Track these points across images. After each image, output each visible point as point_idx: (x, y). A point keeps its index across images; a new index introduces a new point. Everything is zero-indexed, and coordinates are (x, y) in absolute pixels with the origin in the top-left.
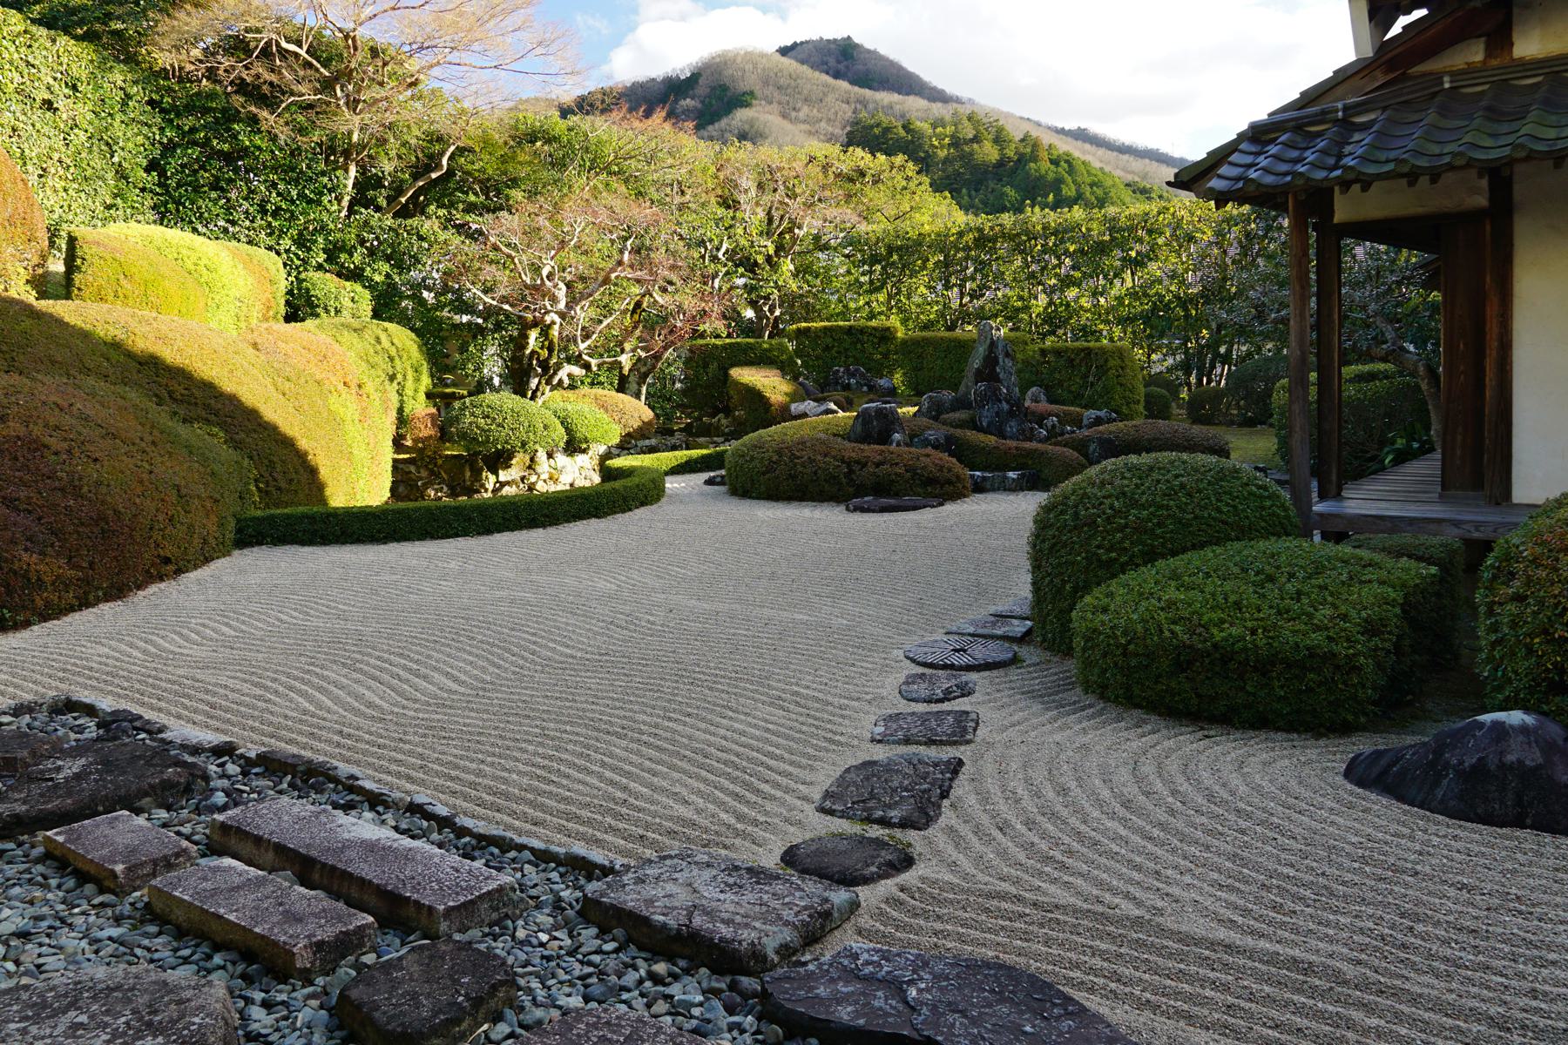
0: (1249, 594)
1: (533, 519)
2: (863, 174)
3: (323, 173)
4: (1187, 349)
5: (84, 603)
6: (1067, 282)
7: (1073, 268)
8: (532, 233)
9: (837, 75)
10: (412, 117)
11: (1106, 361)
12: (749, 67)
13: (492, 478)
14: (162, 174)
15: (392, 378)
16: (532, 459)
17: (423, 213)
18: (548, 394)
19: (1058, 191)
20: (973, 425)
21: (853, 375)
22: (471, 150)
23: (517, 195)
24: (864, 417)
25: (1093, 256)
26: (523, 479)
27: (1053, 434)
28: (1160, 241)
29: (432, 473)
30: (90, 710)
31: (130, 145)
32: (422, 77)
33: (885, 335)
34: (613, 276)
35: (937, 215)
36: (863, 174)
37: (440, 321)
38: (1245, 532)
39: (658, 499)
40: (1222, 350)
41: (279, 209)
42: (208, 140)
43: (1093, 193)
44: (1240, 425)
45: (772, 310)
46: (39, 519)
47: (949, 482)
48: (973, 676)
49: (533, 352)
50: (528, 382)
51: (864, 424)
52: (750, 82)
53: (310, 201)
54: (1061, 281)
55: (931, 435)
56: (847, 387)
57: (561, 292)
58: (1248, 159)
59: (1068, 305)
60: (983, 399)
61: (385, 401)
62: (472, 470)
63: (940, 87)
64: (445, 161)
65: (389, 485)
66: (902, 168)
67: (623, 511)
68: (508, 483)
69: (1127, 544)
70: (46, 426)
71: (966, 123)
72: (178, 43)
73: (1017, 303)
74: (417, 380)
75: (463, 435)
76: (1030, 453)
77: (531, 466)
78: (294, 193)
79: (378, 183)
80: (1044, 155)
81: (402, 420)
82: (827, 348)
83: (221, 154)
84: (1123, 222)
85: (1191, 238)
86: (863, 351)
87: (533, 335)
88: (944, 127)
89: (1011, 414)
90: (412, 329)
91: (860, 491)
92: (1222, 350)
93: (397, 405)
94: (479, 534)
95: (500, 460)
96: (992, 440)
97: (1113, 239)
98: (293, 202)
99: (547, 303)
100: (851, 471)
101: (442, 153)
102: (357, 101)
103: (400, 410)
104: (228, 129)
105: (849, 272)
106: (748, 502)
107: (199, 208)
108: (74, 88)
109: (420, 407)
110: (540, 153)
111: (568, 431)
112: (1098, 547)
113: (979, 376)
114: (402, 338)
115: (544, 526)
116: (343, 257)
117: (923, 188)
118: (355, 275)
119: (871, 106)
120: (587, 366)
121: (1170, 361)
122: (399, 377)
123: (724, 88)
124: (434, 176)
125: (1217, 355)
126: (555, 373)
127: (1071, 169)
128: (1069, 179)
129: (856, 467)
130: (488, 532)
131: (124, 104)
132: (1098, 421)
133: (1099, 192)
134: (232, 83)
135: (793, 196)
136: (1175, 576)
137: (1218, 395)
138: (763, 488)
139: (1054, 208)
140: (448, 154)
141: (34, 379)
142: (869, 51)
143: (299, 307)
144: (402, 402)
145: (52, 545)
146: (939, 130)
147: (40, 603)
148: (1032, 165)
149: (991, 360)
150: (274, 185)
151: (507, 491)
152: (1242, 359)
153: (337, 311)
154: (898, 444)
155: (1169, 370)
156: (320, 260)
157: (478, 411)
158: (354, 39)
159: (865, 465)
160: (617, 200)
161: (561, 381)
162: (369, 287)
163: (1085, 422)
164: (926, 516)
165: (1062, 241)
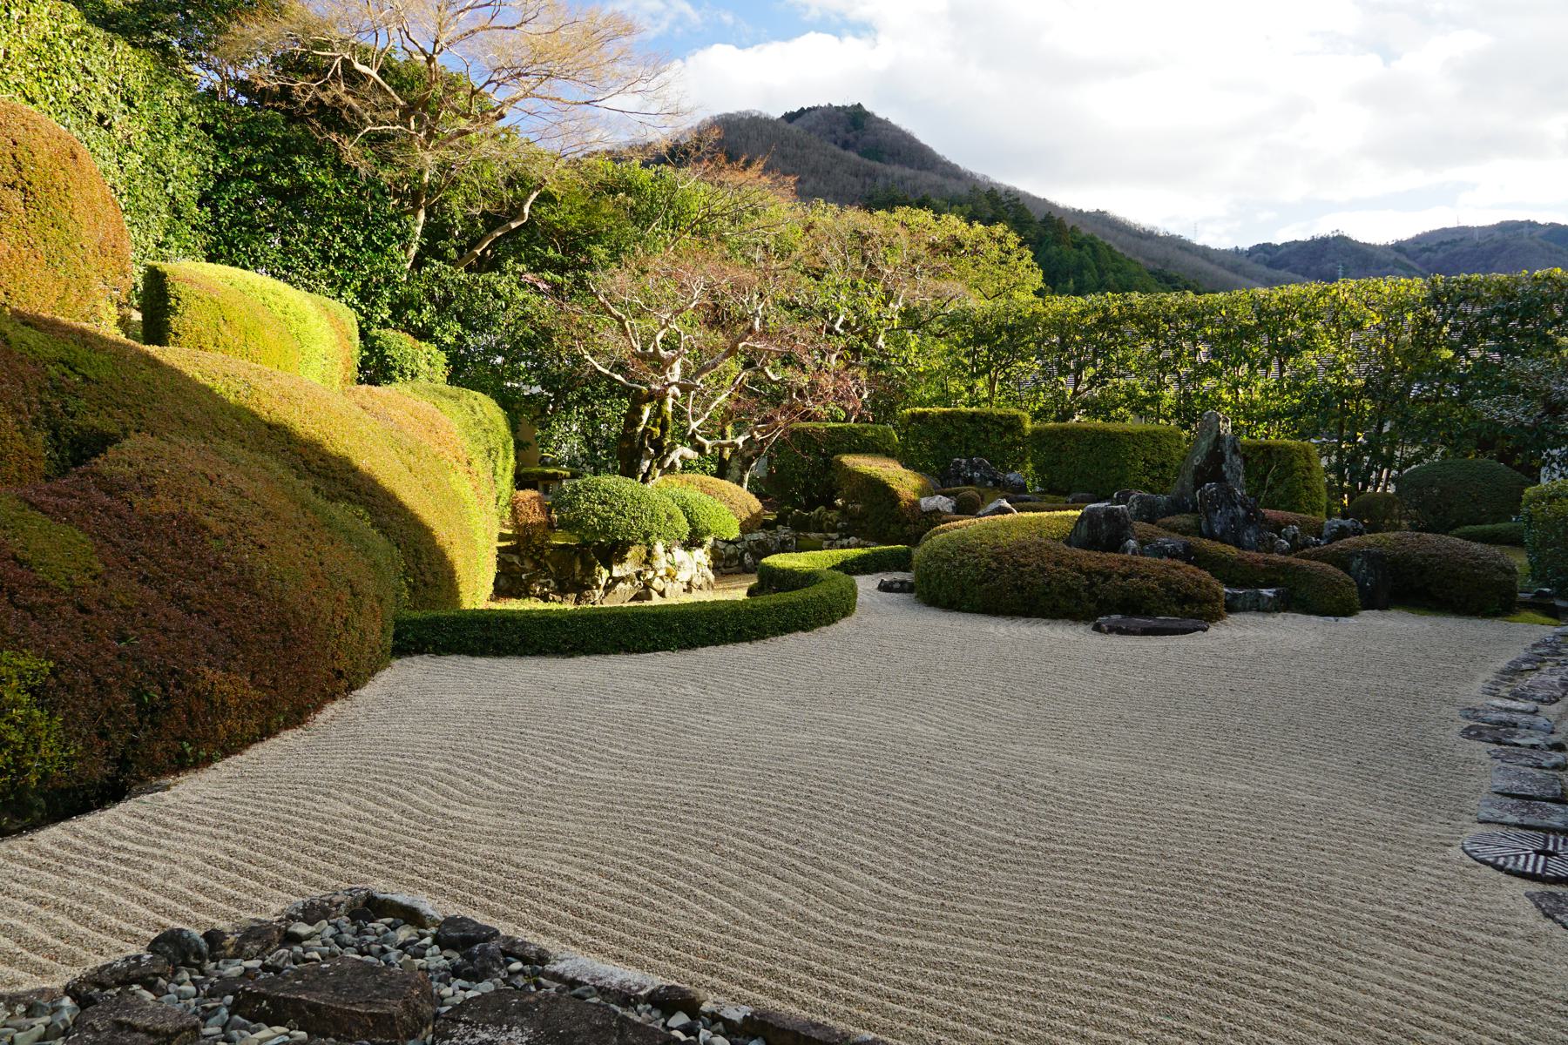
2: (961, 246)
3: (392, 218)
5: (267, 733)
9: (846, 145)
10: (486, 155)
11: (1292, 460)
13: (605, 573)
14: (215, 211)
16: (649, 553)
17: (499, 268)
18: (658, 478)
21: (977, 468)
23: (600, 252)
25: (1232, 343)
26: (639, 574)
27: (1296, 547)
28: (1318, 326)
29: (537, 564)
30: (411, 916)
31: (185, 174)
34: (741, 345)
41: (343, 256)
42: (265, 173)
46: (217, 623)
49: (645, 430)
50: (638, 465)
53: (377, 249)
59: (1205, 397)
62: (582, 563)
63: (953, 162)
64: (526, 210)
68: (622, 579)
70: (200, 501)
72: (252, 50)
76: (1282, 568)
78: (360, 239)
82: (947, 436)
83: (279, 193)
86: (986, 441)
87: (647, 411)
89: (1248, 520)
91: (1105, 607)
94: (681, 648)
95: (613, 552)
96: (1232, 551)
97: (1260, 324)
98: (358, 249)
104: (289, 162)
107: (255, 251)
108: (131, 104)
115: (750, 640)
116: (411, 313)
118: (424, 334)
120: (700, 449)
124: (514, 225)
129: (1098, 579)
131: (179, 126)
134: (309, 104)
138: (978, 600)
139: (1077, 294)
141: (170, 442)
142: (879, 121)
143: (376, 368)
145: (234, 658)
147: (223, 733)
150: (339, 229)
153: (414, 376)
154: (1134, 553)
156: (385, 316)
157: (594, 496)
159: (1107, 577)
161: (673, 464)
163: (1326, 532)
165: (1201, 325)
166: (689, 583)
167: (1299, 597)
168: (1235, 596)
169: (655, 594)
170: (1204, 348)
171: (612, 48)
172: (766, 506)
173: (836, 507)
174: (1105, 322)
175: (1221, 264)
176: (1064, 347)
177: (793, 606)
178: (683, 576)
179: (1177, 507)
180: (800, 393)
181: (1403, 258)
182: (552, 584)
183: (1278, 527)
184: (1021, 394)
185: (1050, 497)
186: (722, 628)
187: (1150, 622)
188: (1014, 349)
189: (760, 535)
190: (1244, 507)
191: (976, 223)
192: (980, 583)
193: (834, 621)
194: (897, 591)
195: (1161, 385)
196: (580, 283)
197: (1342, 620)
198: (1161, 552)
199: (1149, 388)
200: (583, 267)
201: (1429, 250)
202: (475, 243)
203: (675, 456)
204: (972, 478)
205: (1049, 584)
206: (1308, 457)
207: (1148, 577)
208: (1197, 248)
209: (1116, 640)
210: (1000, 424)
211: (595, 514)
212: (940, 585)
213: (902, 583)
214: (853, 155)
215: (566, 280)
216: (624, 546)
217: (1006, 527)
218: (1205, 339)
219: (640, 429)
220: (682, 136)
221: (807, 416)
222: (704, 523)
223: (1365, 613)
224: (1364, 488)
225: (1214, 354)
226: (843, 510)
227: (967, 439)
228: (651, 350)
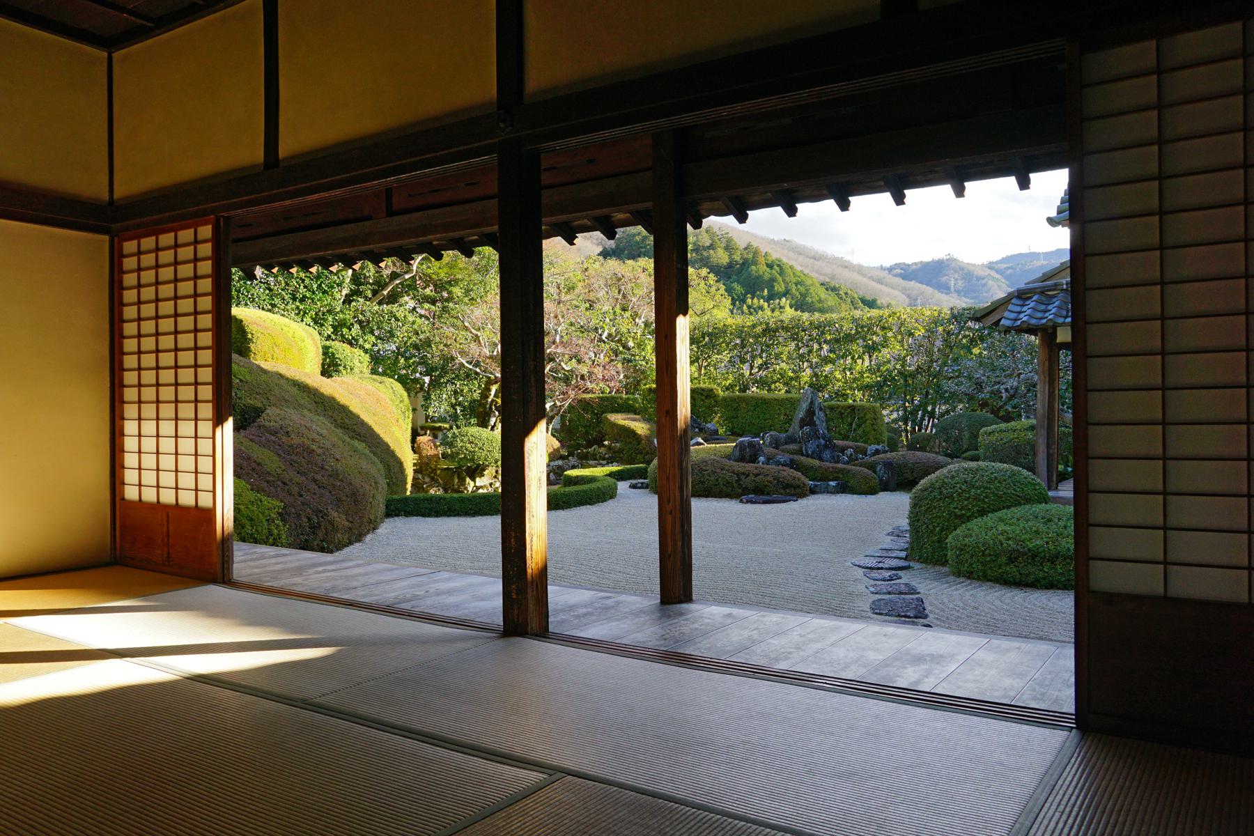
0: (1042, 528)
5: (350, 543)
6: (826, 360)
7: (831, 351)
13: (472, 484)
19: (771, 287)
20: (800, 452)
24: (741, 447)
25: (842, 341)
27: (851, 460)
28: (890, 334)
29: (433, 479)
38: (1028, 501)
40: (929, 408)
41: (304, 297)
47: (799, 487)
48: (900, 573)
53: (325, 292)
58: (1018, 309)
60: (809, 437)
66: (705, 279)
73: (789, 373)
76: (842, 470)
78: (315, 286)
80: (762, 260)
84: (865, 321)
85: (911, 334)
89: (826, 446)
91: (746, 491)
92: (929, 408)
96: (816, 462)
97: (858, 332)
100: (739, 480)
113: (803, 423)
115: (563, 508)
118: (352, 343)
121: (895, 415)
127: (782, 272)
128: (780, 279)
129: (743, 477)
132: (877, 452)
133: (802, 289)
136: (1001, 520)
149: (810, 412)
151: (481, 491)
152: (942, 415)
155: (895, 421)
165: (823, 333)
167: (844, 488)
170: (825, 347)
172: (563, 446)
173: (604, 446)
174: (767, 331)
175: (871, 278)
176: (743, 346)
177: (585, 492)
179: (791, 440)
180: (583, 377)
181: (993, 273)
183: (843, 450)
187: (768, 498)
188: (712, 346)
189: (560, 462)
195: (801, 370)
196: (444, 309)
198: (778, 463)
199: (794, 371)
200: (447, 300)
206: (875, 412)
208: (854, 266)
209: (749, 506)
215: (436, 308)
218: (825, 342)
221: (586, 391)
224: (920, 430)
226: (609, 448)
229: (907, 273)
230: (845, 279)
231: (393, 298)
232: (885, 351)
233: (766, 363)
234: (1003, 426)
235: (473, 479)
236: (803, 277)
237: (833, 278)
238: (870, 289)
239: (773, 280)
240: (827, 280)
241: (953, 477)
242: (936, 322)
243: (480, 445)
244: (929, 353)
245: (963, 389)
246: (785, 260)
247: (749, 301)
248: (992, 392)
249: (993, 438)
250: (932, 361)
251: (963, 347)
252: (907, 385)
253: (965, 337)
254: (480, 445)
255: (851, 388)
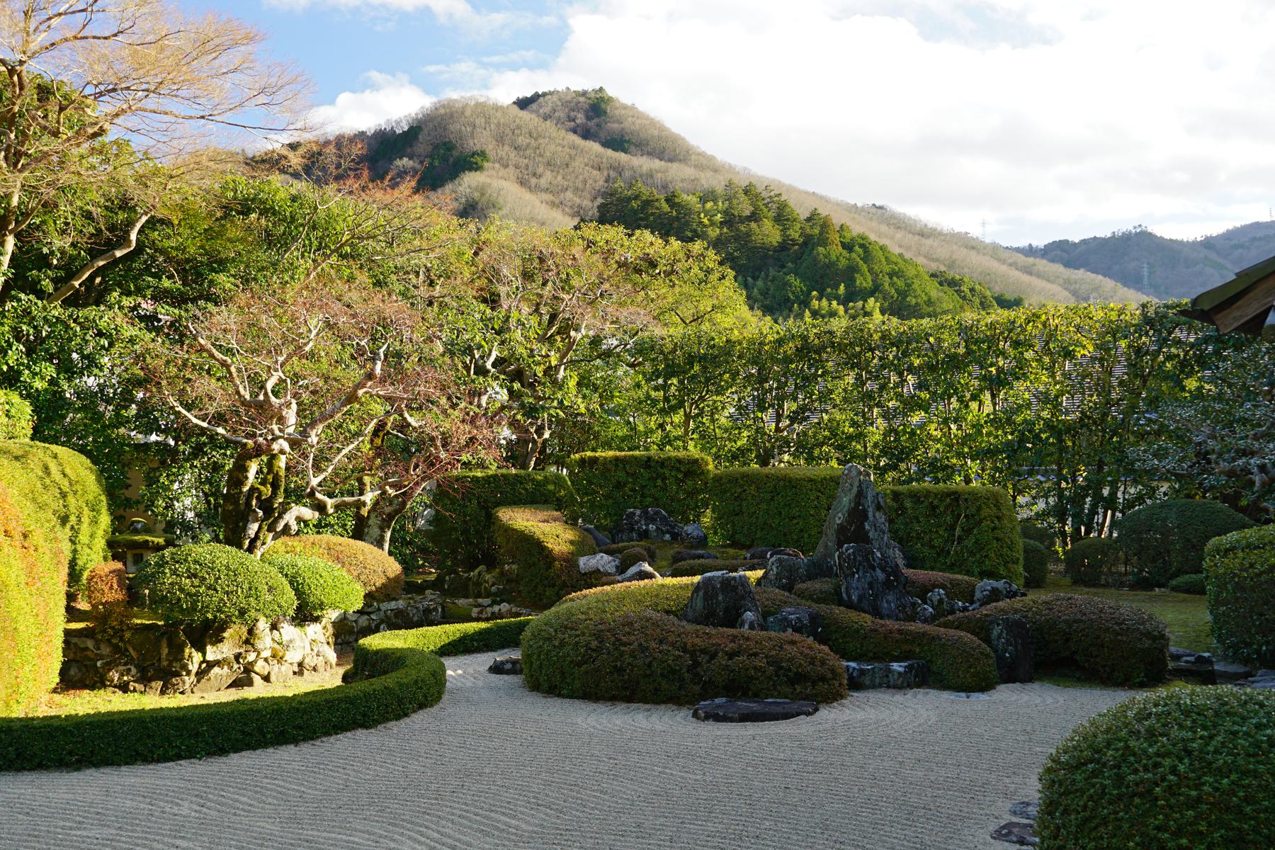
1: (282, 733)
2: (653, 265)
4: (1061, 491)
6: (912, 404)
8: (252, 329)
9: (586, 135)
11: (979, 509)
12: (480, 121)
13: (197, 657)
15: (64, 520)
16: (250, 632)
19: (850, 281)
22: (165, 222)
23: (224, 281)
25: (942, 371)
26: (237, 657)
28: (1029, 355)
29: (116, 649)
32: (107, 126)
33: (691, 468)
34: (361, 392)
35: (737, 319)
36: (653, 265)
37: (124, 442)
39: (438, 698)
40: (1106, 492)
43: (892, 284)
44: (1133, 587)
45: (540, 431)
47: (823, 679)
49: (252, 489)
50: (245, 529)
51: (705, 599)
52: (482, 140)
54: (905, 403)
55: (792, 613)
56: (645, 535)
57: (291, 416)
59: (913, 433)
61: (57, 553)
62: (170, 646)
63: (709, 152)
64: (133, 236)
65: (58, 666)
67: (398, 718)
68: (217, 663)
69: (1203, 827)
71: (742, 197)
73: (848, 433)
74: (94, 522)
75: (158, 600)
77: (249, 640)
79: (43, 262)
80: (835, 237)
81: (74, 575)
82: (619, 486)
85: (1069, 354)
86: (664, 489)
87: (253, 467)
88: (715, 201)
90: (82, 450)
91: (709, 690)
92: (1106, 492)
93: (69, 556)
94: (210, 754)
96: (867, 620)
97: (969, 352)
99: (275, 427)
100: (696, 664)
101: (130, 224)
102: (19, 155)
103: (73, 563)
105: (638, 386)
106: (558, 702)
109: (96, 559)
110: (248, 230)
111: (299, 593)
112: (1158, 828)
113: (843, 535)
114: (75, 466)
115: (295, 741)
117: (727, 282)
119: (627, 174)
120: (320, 507)
121: (1041, 505)
122: (73, 519)
123: (449, 146)
124: (118, 254)
125: (1098, 498)
126: (280, 516)
127: (867, 256)
128: (865, 268)
129: (703, 659)
130: (222, 751)
132: (995, 595)
133: (900, 283)
135: (566, 284)
137: (1106, 547)
138: (577, 684)
140: (138, 225)
142: (625, 107)
144: (75, 551)
146: (709, 205)
148: (821, 249)
149: (858, 514)
152: (1129, 504)
154: (752, 627)
155: (1041, 516)
157: (182, 569)
158: (19, 76)
159: (713, 656)
160: (362, 299)
161: (287, 527)
162: (28, 396)
163: (978, 595)
164: (801, 727)
165: (905, 354)
166: (300, 665)
167: (925, 676)
168: (862, 672)
169: (257, 679)
170: (911, 379)
171: (229, 59)
178: (293, 656)
179: (819, 570)
181: (1214, 256)
182: (134, 671)
183: (923, 591)
184: (713, 433)
185: (731, 551)
186: (260, 730)
187: (754, 706)
188: (710, 382)
190: (883, 570)
191: (672, 240)
192: (579, 665)
193: (406, 715)
194: (508, 672)
197: (975, 696)
199: (854, 424)
201: (1242, 246)
202: (72, 275)
203: (290, 518)
204: (646, 531)
205: (649, 665)
207: (756, 655)
208: (986, 246)
210: (678, 470)
211: (182, 590)
212: (540, 667)
213: (514, 662)
214: (595, 147)
216: (223, 626)
217: (620, 598)
218: (911, 369)
219: (245, 489)
220: (398, 123)
222: (316, 594)
223: (1002, 687)
224: (1088, 532)
225: (921, 386)
227: (643, 487)
228: (261, 397)
229: (1065, 253)
230: (972, 266)
231: (94, 295)
232: (1020, 386)
233: (803, 409)
234: (1251, 533)
235: (203, 651)
236: (902, 265)
237: (951, 265)
238: (1012, 279)
239: (852, 270)
240: (943, 268)
241: (1151, 735)
242: (1115, 330)
243: (210, 580)
244: (1103, 388)
245: (1169, 464)
246: (872, 237)
247: (815, 304)
248: (1230, 474)
249: (1233, 562)
250: (1109, 403)
251: (1166, 377)
252: (1063, 449)
253: (1169, 358)
254: (210, 580)
255: (960, 455)
